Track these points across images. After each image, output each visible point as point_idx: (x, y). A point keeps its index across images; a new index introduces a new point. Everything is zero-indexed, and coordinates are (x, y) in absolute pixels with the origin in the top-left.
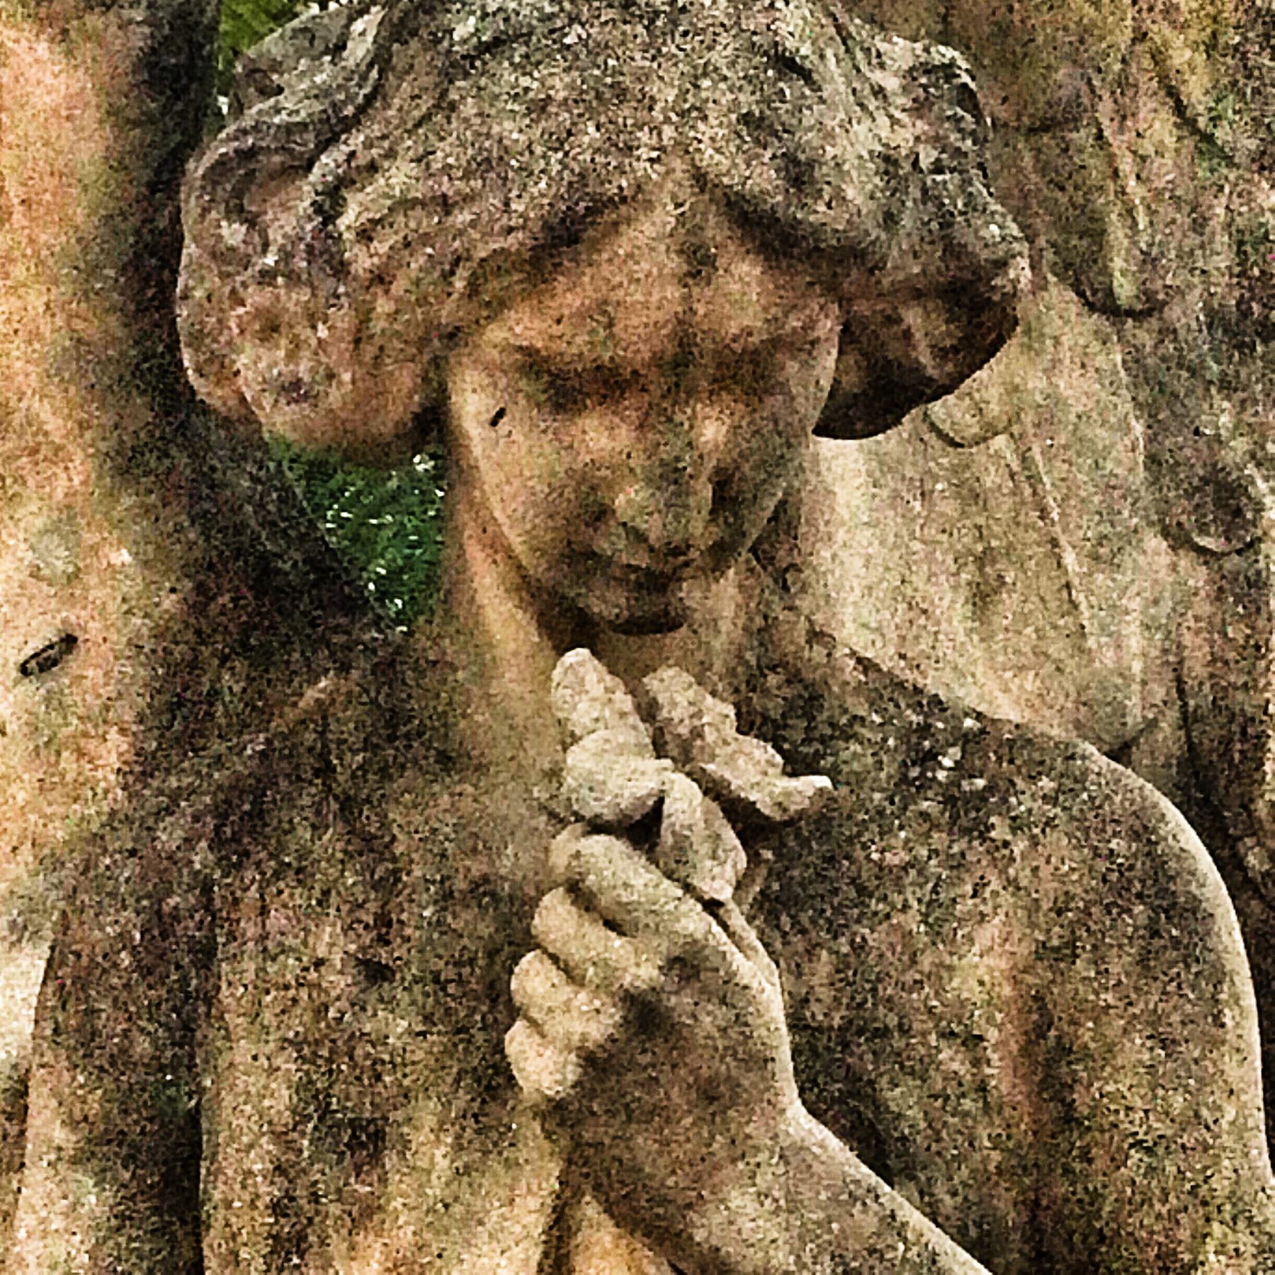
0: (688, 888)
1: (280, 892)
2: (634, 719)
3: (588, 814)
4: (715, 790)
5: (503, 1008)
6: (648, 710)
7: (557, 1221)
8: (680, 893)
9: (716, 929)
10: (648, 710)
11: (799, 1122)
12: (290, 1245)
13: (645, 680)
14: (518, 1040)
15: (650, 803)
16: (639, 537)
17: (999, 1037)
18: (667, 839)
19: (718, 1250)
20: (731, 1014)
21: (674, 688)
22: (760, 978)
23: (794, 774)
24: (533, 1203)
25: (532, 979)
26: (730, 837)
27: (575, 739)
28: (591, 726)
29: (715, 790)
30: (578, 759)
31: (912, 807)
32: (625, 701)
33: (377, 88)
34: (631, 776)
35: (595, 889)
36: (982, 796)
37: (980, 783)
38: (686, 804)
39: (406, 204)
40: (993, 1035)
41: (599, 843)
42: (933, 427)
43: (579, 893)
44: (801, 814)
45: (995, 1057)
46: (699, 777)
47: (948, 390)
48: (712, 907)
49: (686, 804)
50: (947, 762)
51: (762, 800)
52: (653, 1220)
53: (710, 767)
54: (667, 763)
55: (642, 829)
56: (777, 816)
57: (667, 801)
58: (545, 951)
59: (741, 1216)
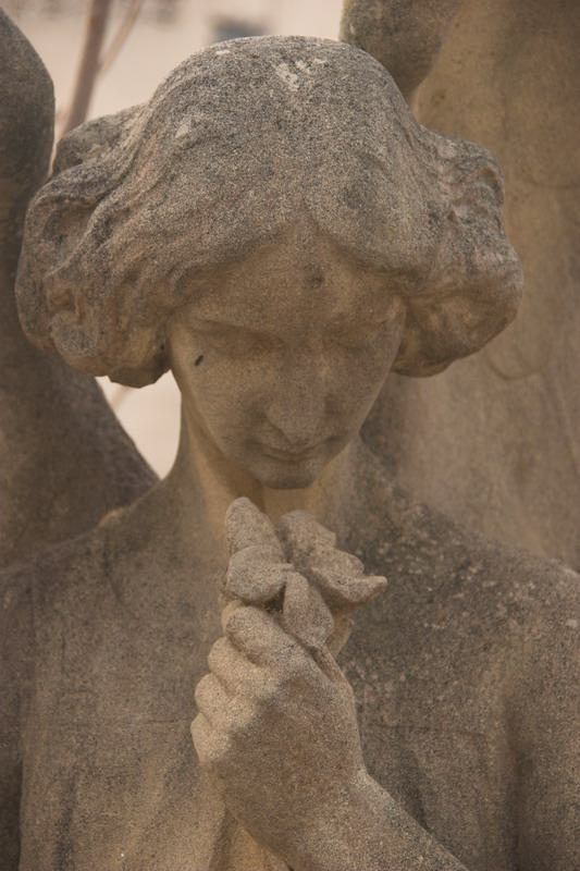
0: (299, 641)
1: (74, 635)
2: (275, 539)
3: (240, 593)
4: (316, 583)
5: (191, 707)
6: (283, 535)
7: (223, 836)
8: (292, 642)
9: (313, 664)
10: (283, 535)
11: (363, 779)
12: (61, 863)
13: (284, 517)
14: (198, 728)
15: (278, 588)
16: (280, 433)
17: (495, 733)
18: (287, 610)
19: (310, 856)
20: (320, 715)
21: (304, 526)
22: (343, 694)
23: (366, 573)
24: (208, 825)
25: (206, 691)
26: (325, 611)
27: (237, 550)
28: (247, 542)
29: (316, 583)
30: (236, 562)
31: (450, 597)
32: (267, 526)
33: (132, 165)
34: (270, 575)
35: (243, 639)
36: (491, 590)
37: (492, 584)
38: (298, 591)
39: (142, 235)
40: (492, 736)
41: (245, 612)
42: (492, 367)
43: (236, 644)
44: (367, 598)
45: (493, 748)
46: (308, 575)
47: (475, 350)
48: (312, 652)
49: (298, 591)
50: (474, 570)
51: (345, 590)
52: (279, 841)
53: (315, 569)
54: (290, 566)
55: (273, 604)
56: (355, 600)
57: (288, 588)
58: (215, 674)
59: (328, 837)
